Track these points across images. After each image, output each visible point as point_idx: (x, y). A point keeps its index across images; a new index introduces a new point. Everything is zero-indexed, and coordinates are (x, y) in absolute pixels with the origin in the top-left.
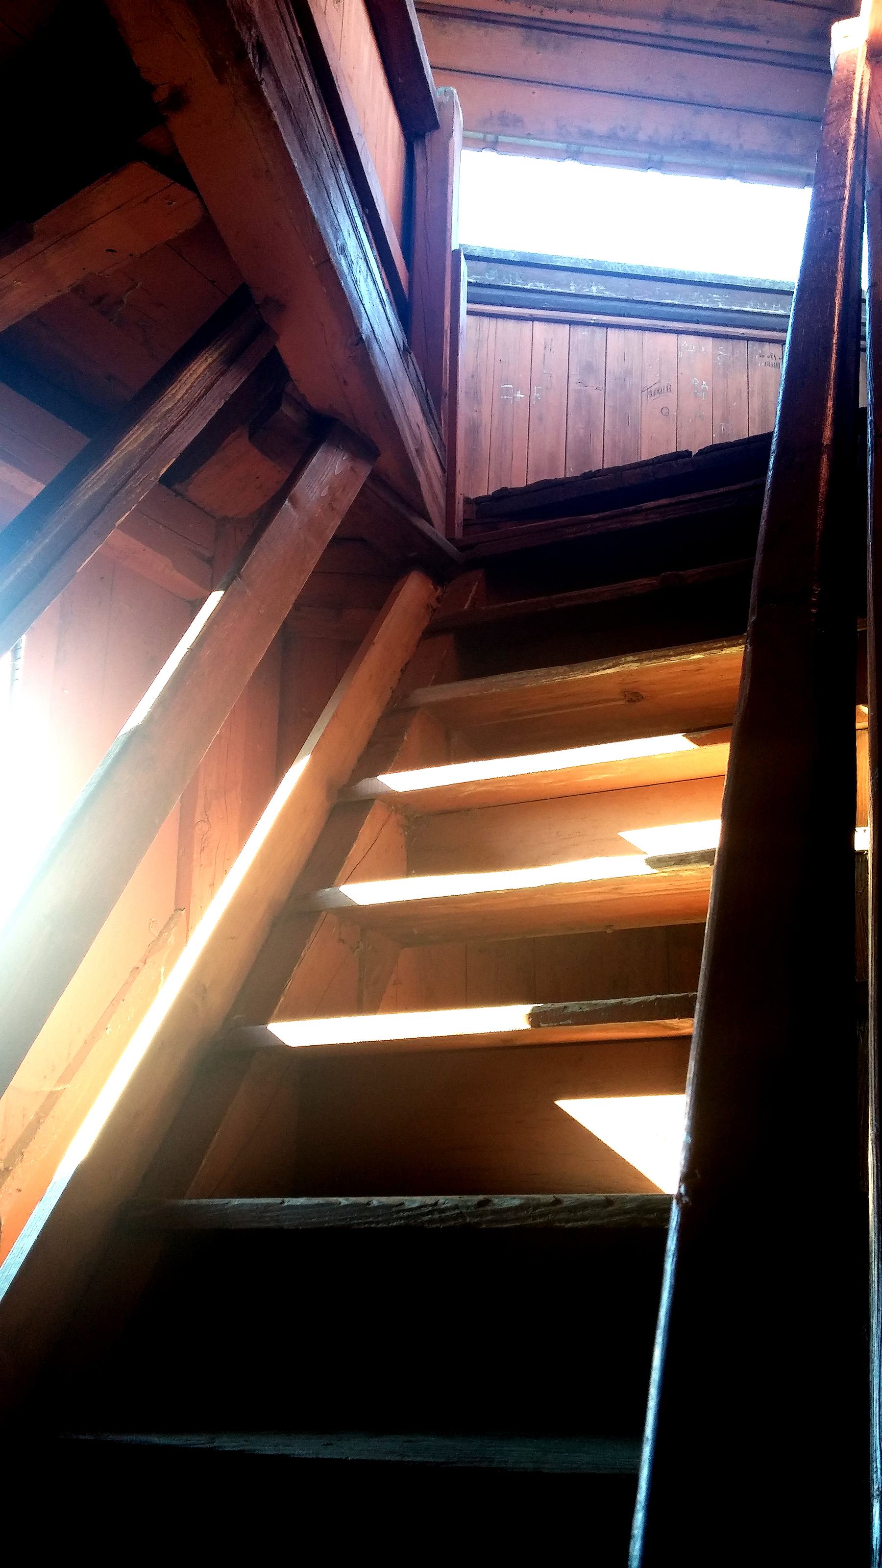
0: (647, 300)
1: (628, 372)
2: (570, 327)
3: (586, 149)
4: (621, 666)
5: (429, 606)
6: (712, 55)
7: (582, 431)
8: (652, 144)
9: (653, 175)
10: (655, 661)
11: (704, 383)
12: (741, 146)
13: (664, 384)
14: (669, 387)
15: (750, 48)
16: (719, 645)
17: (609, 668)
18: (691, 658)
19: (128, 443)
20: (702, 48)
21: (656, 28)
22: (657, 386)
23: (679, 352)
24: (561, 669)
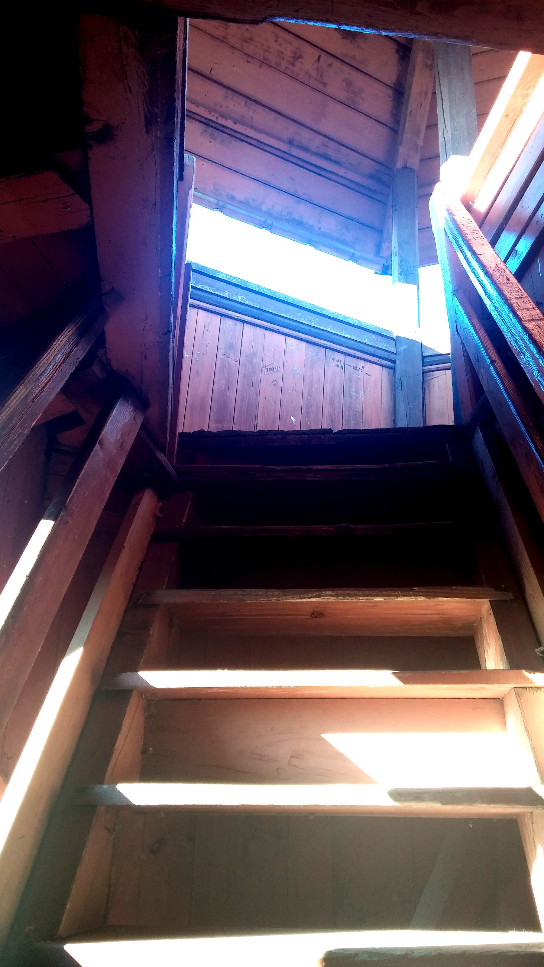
0: (271, 311)
1: (254, 354)
2: (221, 319)
3: (229, 206)
4: (322, 598)
5: (155, 515)
6: (312, 171)
7: (223, 386)
8: (269, 214)
9: (265, 232)
10: (348, 598)
11: (299, 369)
12: (320, 229)
13: (275, 365)
14: (278, 368)
15: (334, 173)
16: (395, 593)
17: (313, 597)
18: (374, 600)
19: (14, 402)
20: (306, 166)
21: (284, 147)
22: (271, 366)
23: (286, 347)
24: (276, 592)
